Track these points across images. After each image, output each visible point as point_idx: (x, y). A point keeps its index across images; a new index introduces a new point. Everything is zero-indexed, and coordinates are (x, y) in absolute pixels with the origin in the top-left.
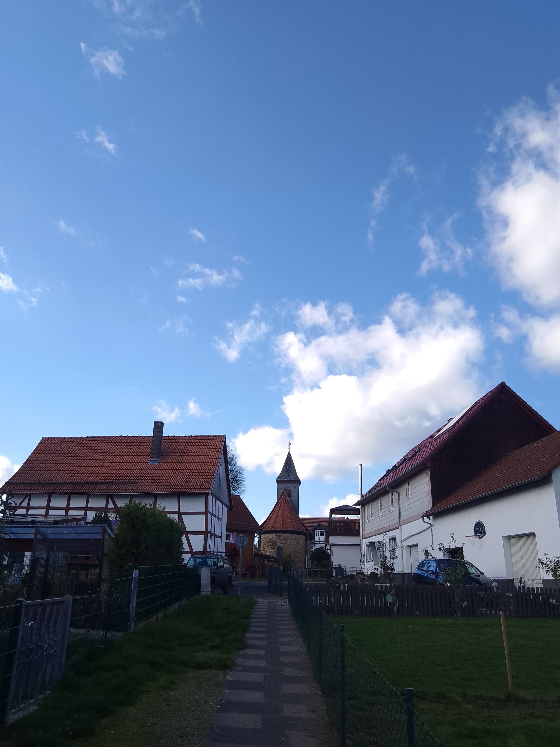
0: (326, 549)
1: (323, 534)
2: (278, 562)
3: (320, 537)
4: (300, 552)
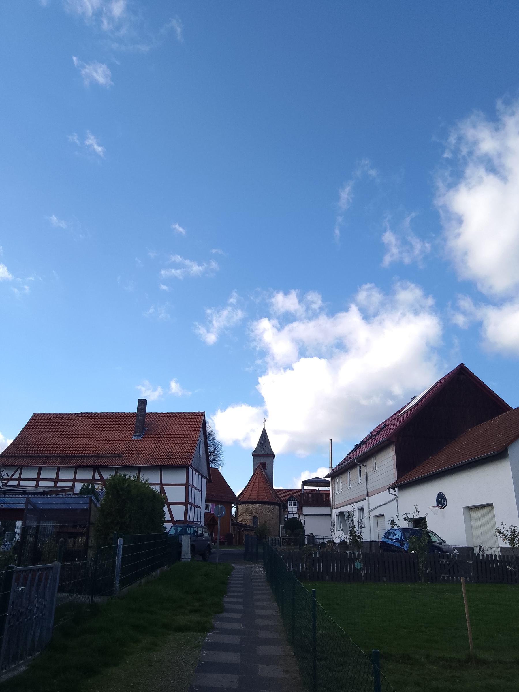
0: (299, 518)
1: (296, 504)
2: (254, 530)
3: (293, 507)
4: (274, 521)
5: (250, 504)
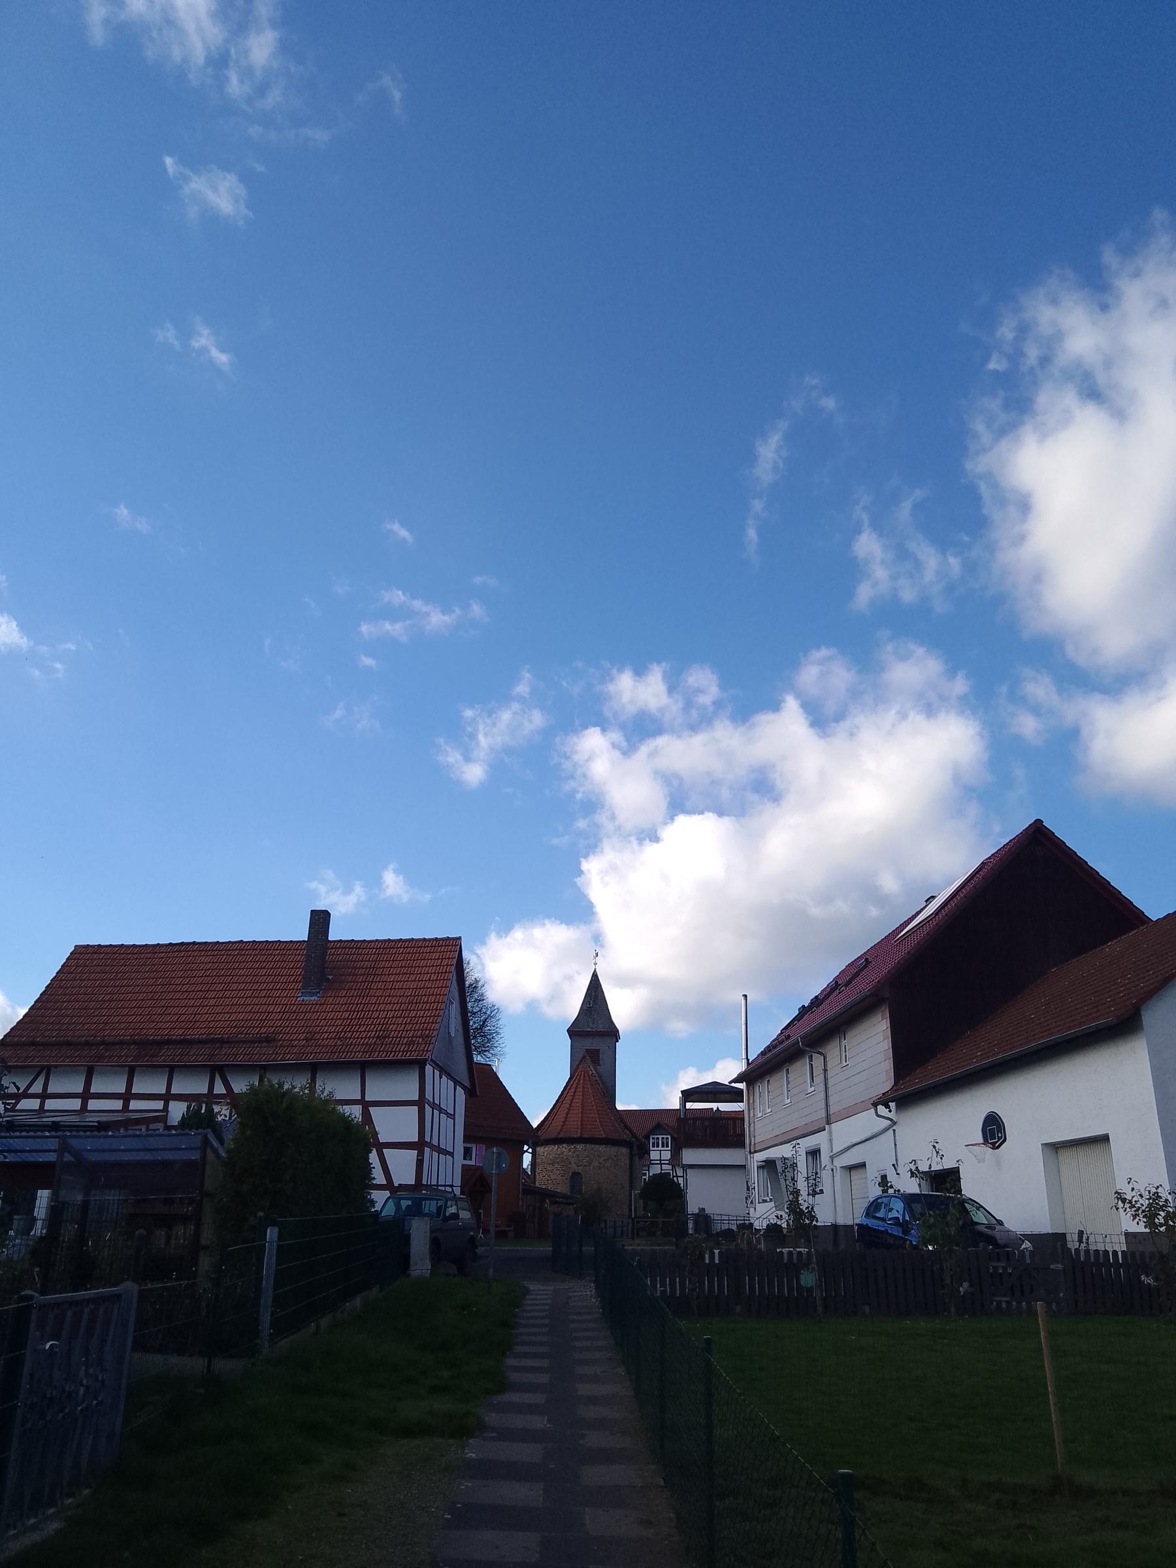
0: (675, 1175)
1: (667, 1143)
2: (572, 1204)
3: (660, 1151)
5: (564, 1145)
